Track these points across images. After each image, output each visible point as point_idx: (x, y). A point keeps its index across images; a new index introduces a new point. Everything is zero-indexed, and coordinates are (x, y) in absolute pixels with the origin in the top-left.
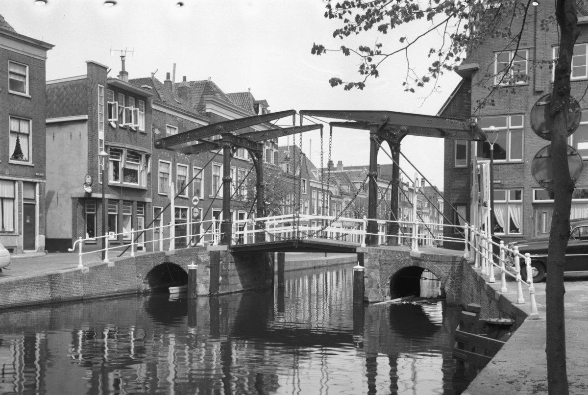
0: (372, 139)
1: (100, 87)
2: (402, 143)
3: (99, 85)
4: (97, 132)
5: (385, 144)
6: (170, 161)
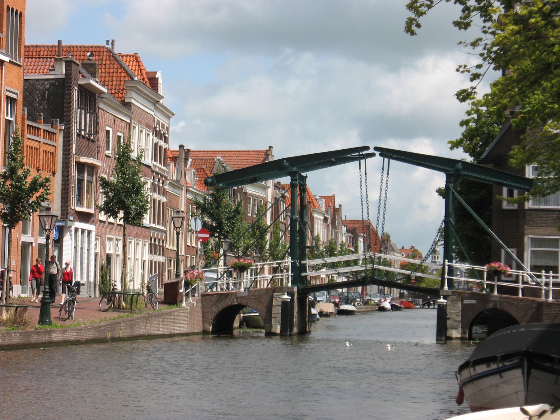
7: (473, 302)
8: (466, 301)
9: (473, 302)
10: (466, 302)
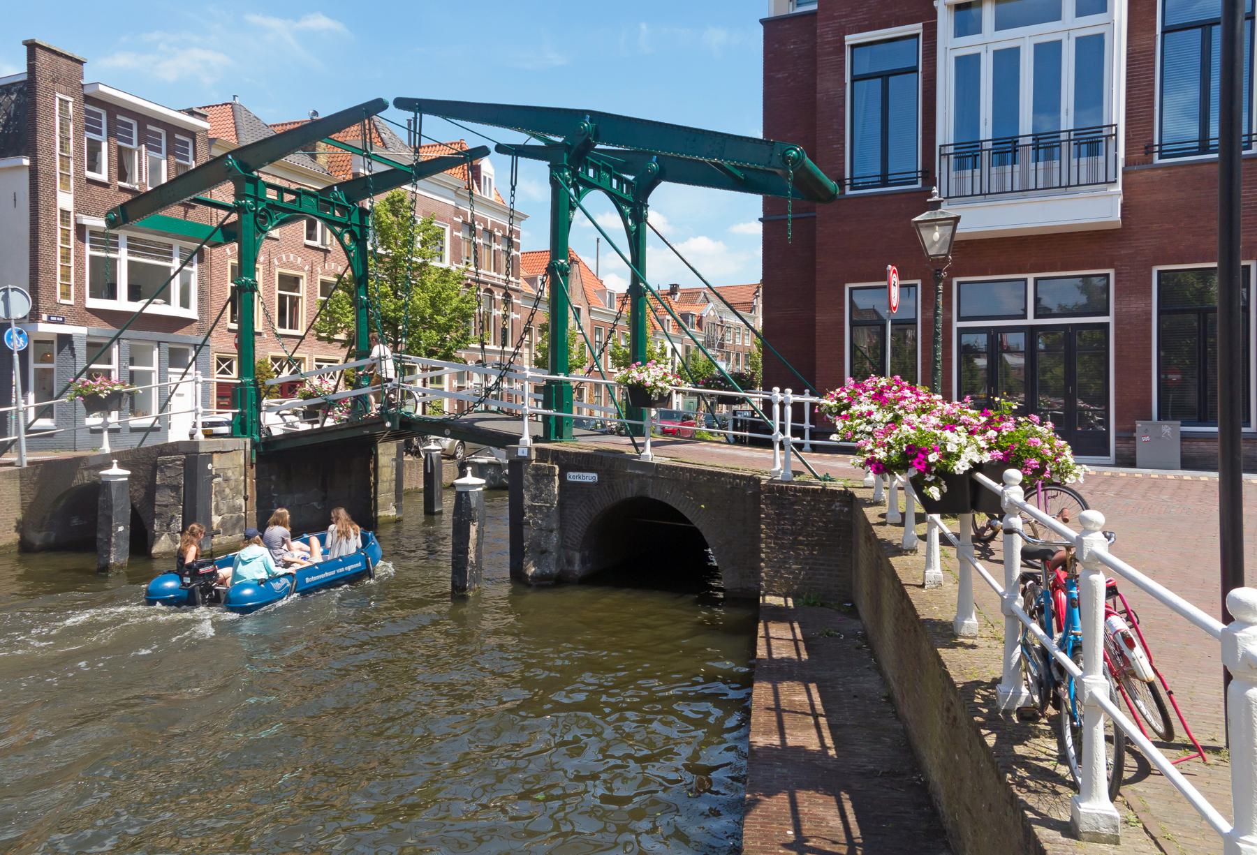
0: (553, 181)
1: (60, 99)
2: (651, 199)
3: (58, 95)
4: (55, 193)
5: (597, 201)
6: (304, 271)
7: (590, 477)
8: (571, 474)
9: (590, 477)
10: (573, 476)
